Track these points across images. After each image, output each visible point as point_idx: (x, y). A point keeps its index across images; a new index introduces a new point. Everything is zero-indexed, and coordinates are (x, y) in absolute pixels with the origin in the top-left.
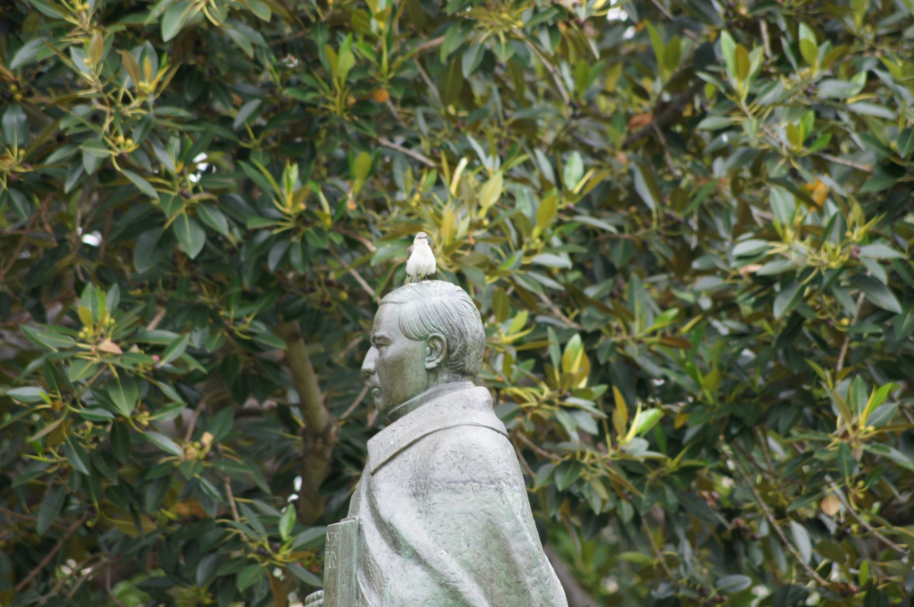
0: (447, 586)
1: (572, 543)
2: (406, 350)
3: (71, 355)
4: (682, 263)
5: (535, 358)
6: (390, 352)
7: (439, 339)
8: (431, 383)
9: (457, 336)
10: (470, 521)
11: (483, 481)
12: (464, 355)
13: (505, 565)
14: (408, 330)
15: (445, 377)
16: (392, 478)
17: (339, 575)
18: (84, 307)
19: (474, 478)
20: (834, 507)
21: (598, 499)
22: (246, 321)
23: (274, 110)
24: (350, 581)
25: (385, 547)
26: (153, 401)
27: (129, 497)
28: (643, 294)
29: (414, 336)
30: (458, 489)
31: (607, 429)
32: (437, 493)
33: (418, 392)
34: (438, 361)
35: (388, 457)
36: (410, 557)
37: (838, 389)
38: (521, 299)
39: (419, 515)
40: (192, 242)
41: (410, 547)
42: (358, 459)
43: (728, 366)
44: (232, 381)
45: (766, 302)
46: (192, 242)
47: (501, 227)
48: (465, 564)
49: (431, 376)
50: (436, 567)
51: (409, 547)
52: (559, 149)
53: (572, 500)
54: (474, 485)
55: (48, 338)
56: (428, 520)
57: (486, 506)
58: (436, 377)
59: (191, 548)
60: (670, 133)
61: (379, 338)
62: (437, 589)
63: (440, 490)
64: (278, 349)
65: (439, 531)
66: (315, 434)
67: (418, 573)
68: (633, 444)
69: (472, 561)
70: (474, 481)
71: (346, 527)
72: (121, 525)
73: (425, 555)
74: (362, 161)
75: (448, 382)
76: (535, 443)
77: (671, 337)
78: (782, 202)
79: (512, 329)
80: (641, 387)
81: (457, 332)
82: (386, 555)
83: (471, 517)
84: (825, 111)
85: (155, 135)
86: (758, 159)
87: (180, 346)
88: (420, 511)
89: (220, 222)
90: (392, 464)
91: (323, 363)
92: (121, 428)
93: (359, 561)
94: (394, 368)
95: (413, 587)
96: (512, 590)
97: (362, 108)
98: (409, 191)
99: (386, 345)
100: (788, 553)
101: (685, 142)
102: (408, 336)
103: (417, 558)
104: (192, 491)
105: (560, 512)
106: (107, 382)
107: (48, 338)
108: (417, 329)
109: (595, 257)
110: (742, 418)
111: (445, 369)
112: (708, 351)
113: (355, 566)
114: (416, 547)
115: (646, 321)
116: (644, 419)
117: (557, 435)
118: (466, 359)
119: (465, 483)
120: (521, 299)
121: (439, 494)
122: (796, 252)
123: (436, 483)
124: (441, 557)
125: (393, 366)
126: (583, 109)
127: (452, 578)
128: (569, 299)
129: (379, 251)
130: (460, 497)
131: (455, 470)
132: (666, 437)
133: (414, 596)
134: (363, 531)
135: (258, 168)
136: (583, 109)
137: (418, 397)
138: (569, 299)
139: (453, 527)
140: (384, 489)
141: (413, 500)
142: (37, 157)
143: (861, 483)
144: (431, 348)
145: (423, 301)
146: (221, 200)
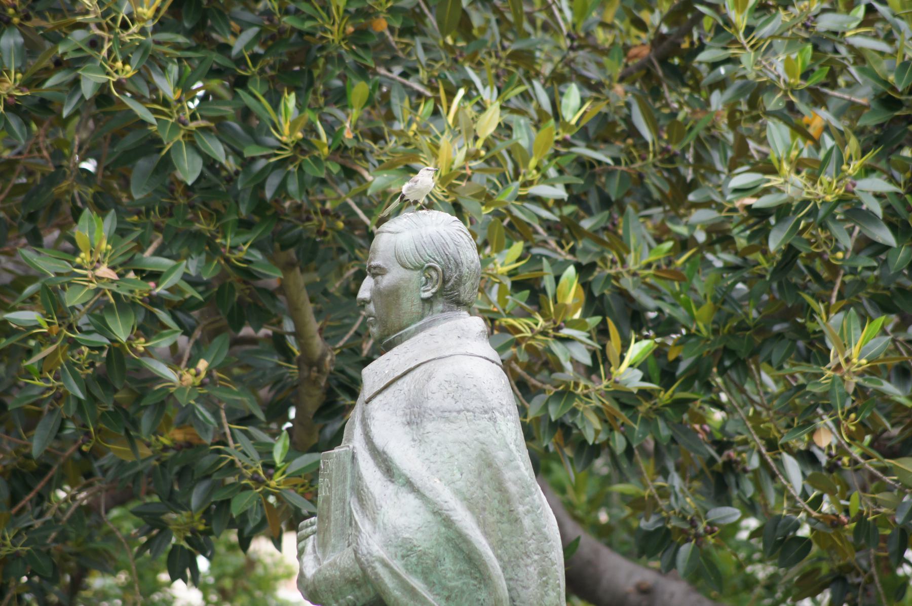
0: (440, 515)
1: (566, 473)
2: (402, 279)
3: (68, 280)
4: (678, 195)
5: (529, 288)
6: (386, 281)
7: (435, 269)
9: (452, 266)
10: (463, 450)
11: (477, 410)
12: (459, 285)
13: (497, 494)
14: (404, 259)
16: (387, 406)
18: (81, 232)
20: (825, 439)
21: (591, 429)
22: (242, 248)
23: (272, 38)
24: (344, 508)
26: (149, 327)
27: (124, 421)
28: (637, 228)
29: (410, 266)
31: (600, 362)
33: (413, 321)
34: (434, 290)
35: (382, 386)
36: (404, 485)
37: (832, 322)
38: (517, 229)
39: (412, 443)
40: (189, 169)
41: (404, 475)
42: (353, 388)
43: (723, 298)
44: (229, 308)
45: (762, 234)
46: (189, 169)
47: (499, 158)
48: (457, 492)
49: (426, 305)
52: (558, 80)
53: (564, 430)
55: (47, 264)
57: (480, 435)
58: (431, 307)
59: (186, 474)
60: (668, 65)
61: (375, 268)
62: (430, 517)
63: (434, 419)
64: (274, 277)
66: (310, 362)
67: (410, 501)
68: (627, 375)
69: (464, 490)
70: (468, 411)
72: (117, 450)
73: (418, 484)
74: (360, 90)
75: (442, 312)
76: (529, 373)
77: (666, 270)
78: (778, 135)
79: (507, 259)
80: (635, 320)
82: (379, 483)
83: (464, 446)
84: (822, 44)
85: (153, 61)
86: (755, 92)
87: (177, 273)
89: (217, 150)
91: (318, 293)
92: (117, 353)
93: (352, 488)
94: (390, 297)
96: (505, 519)
97: (361, 37)
98: (407, 120)
99: (382, 275)
101: (680, 76)
102: (404, 266)
103: (411, 486)
104: (188, 418)
105: (553, 442)
106: (103, 307)
107: (47, 264)
108: (411, 258)
109: (591, 189)
110: (734, 351)
111: (440, 299)
112: (702, 284)
113: (348, 493)
114: (409, 475)
115: (641, 253)
116: (638, 349)
117: (552, 365)
119: (459, 412)
120: (517, 229)
121: (433, 423)
122: (792, 185)
123: (430, 412)
125: (388, 296)
126: (581, 41)
128: (565, 231)
129: (376, 180)
130: (454, 426)
131: (449, 400)
132: (661, 368)
133: (407, 524)
134: (357, 459)
135: (255, 97)
136: (581, 41)
137: (413, 327)
138: (565, 231)
139: (447, 455)
140: (380, 419)
141: (407, 428)
142: (33, 81)
143: (853, 416)
144: (427, 278)
145: (416, 234)
146: (219, 127)
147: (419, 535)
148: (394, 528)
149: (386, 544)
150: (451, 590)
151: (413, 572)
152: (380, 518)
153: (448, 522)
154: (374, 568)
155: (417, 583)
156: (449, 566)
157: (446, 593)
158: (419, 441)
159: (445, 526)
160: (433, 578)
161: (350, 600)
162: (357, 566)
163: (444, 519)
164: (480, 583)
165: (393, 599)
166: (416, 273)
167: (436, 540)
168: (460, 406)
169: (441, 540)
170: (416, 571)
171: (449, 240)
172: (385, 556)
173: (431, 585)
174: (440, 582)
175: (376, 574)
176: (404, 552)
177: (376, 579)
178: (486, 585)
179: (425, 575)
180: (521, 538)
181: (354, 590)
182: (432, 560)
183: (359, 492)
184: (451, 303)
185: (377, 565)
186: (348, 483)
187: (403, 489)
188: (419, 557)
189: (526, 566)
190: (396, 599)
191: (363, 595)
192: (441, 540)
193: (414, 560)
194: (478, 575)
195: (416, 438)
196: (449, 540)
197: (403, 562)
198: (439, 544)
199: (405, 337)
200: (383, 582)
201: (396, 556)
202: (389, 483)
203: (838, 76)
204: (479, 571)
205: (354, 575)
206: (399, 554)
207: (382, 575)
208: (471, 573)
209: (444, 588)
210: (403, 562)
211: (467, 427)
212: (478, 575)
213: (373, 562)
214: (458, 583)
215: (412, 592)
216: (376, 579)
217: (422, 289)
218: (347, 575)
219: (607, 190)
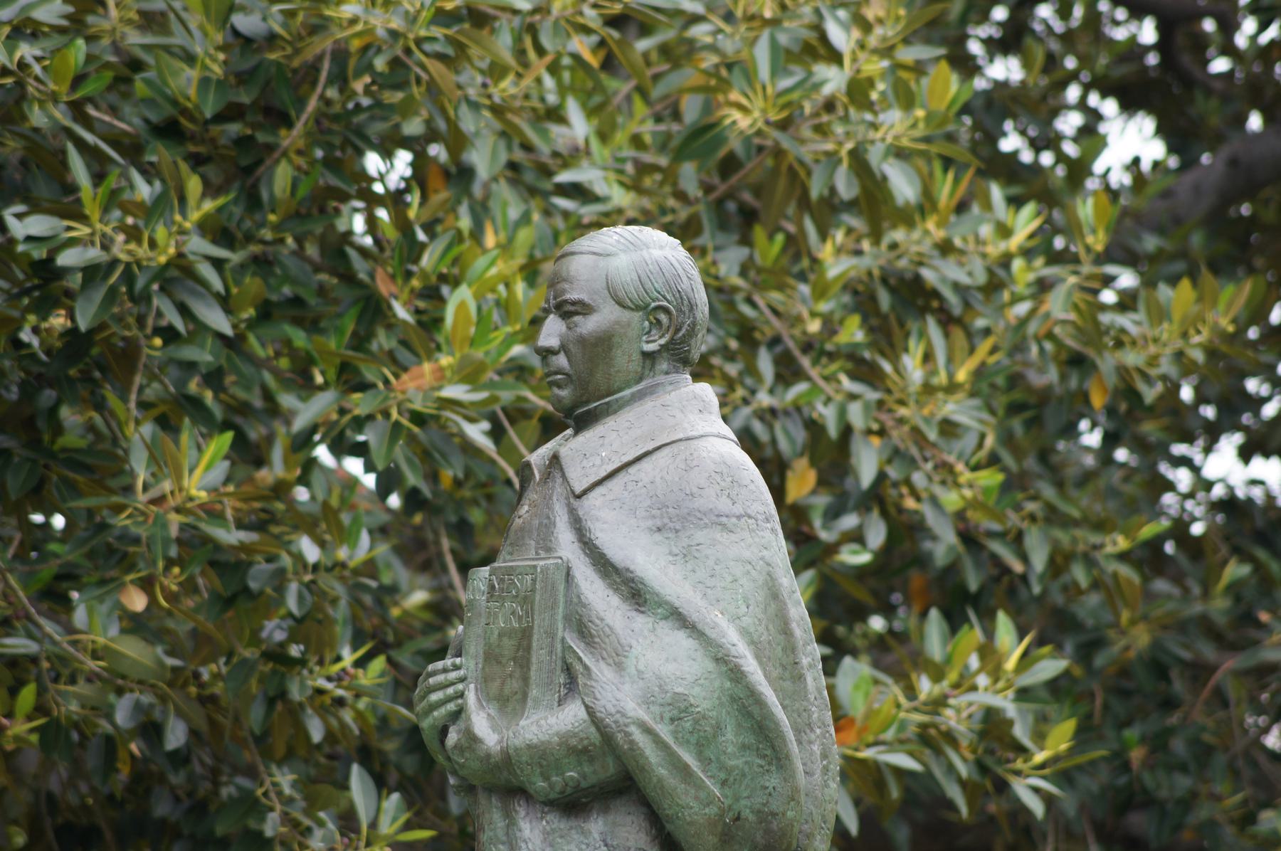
0: (726, 662)
2: (617, 323)
6: (589, 325)
7: (666, 311)
8: (647, 372)
9: (685, 309)
10: (748, 572)
11: (759, 517)
12: (691, 337)
13: (782, 637)
14: (621, 294)
15: (664, 366)
16: (616, 504)
17: (535, 637)
19: (749, 512)
24: (552, 646)
25: (615, 600)
29: (630, 304)
30: (730, 525)
32: (701, 529)
33: (628, 386)
34: (663, 341)
35: (603, 474)
36: (666, 618)
39: (671, 558)
41: (667, 603)
48: (744, 632)
49: (648, 362)
50: (712, 634)
51: (661, 603)
54: (750, 521)
56: (689, 566)
57: (765, 553)
58: (653, 365)
61: (574, 303)
62: (710, 665)
63: (706, 526)
65: (710, 582)
67: (681, 641)
69: (752, 630)
70: (750, 517)
71: (548, 569)
73: (694, 617)
75: (667, 373)
81: (686, 302)
82: (619, 613)
83: (749, 567)
88: (670, 553)
90: (611, 484)
93: (567, 618)
95: (675, 660)
96: (787, 674)
99: (584, 314)
100: (831, 680)
102: (620, 304)
103: (679, 618)
108: (634, 294)
111: (665, 354)
113: (560, 626)
114: (677, 604)
118: (693, 342)
119: (739, 517)
121: (705, 531)
123: (699, 515)
124: (716, 620)
125: (595, 345)
127: (733, 651)
130: (733, 537)
131: (724, 499)
133: (678, 673)
134: (573, 577)
137: (627, 392)
139: (730, 579)
141: (658, 537)
143: (176, 570)
144: (651, 323)
147: (697, 690)
148: (659, 678)
149: (647, 701)
150: (729, 771)
151: (685, 743)
152: (630, 664)
153: (736, 674)
154: (627, 734)
155: (688, 758)
156: (730, 737)
157: (723, 776)
158: (687, 555)
159: (731, 680)
160: (709, 753)
161: (572, 777)
162: (593, 729)
163: (731, 670)
164: (770, 764)
165: (655, 780)
166: (637, 316)
167: (719, 698)
168: (738, 509)
169: (724, 699)
170: (688, 742)
171: (681, 271)
172: (646, 718)
173: (705, 761)
174: (718, 759)
175: (632, 742)
176: (675, 712)
177: (631, 749)
178: (781, 767)
179: (700, 749)
180: (805, 703)
181: (580, 764)
182: (712, 727)
183: (582, 626)
184: (677, 361)
185: (633, 729)
186: (560, 611)
187: (663, 623)
188: (696, 722)
189: (810, 742)
190: (660, 780)
191: (594, 772)
192: (724, 699)
193: (688, 725)
194: (768, 752)
195: (675, 550)
196: (733, 699)
197: (672, 727)
198: (721, 704)
199: (615, 407)
200: (642, 754)
201: (662, 718)
202: (634, 614)
203: (1275, 63)
204: (773, 748)
205: (586, 742)
206: (667, 716)
207: (641, 745)
208: (758, 749)
209: (722, 767)
210: (672, 727)
211: (750, 540)
212: (768, 752)
213: (626, 725)
214: (738, 762)
215: (684, 771)
216: (631, 749)
217: (644, 338)
218: (573, 742)
219: (585, 163)
